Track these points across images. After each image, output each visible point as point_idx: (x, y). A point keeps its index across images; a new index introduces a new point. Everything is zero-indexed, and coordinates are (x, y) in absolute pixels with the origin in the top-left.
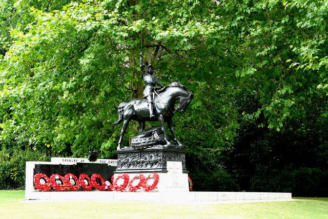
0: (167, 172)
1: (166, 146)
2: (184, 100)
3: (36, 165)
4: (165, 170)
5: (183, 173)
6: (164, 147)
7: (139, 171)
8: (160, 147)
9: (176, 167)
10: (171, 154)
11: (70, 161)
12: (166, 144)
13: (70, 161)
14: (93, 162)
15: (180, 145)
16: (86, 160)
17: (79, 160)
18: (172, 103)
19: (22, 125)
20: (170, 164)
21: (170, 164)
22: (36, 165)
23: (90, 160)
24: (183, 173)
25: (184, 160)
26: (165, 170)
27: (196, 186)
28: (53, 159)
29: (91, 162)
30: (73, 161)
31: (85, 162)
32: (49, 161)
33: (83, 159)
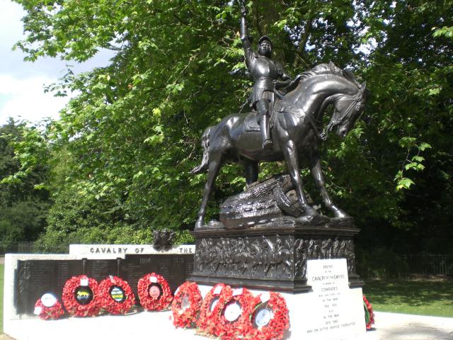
0: (308, 289)
1: (305, 219)
2: (349, 102)
3: (20, 263)
4: (300, 285)
5: (351, 286)
6: (298, 223)
7: (257, 285)
8: (292, 223)
9: (329, 273)
10: (316, 238)
11: (98, 251)
12: (304, 213)
13: (109, 251)
14: (165, 253)
15: (341, 215)
16: (149, 249)
17: (132, 249)
18: (289, 118)
19: (378, 8)
20: (315, 268)
21: (315, 268)
22: (20, 263)
23: (157, 248)
24: (351, 286)
25: (352, 255)
26: (300, 285)
27: (373, 323)
28: (72, 247)
29: (160, 253)
30: (117, 250)
31: (144, 253)
32: (66, 251)
33: (139, 247)
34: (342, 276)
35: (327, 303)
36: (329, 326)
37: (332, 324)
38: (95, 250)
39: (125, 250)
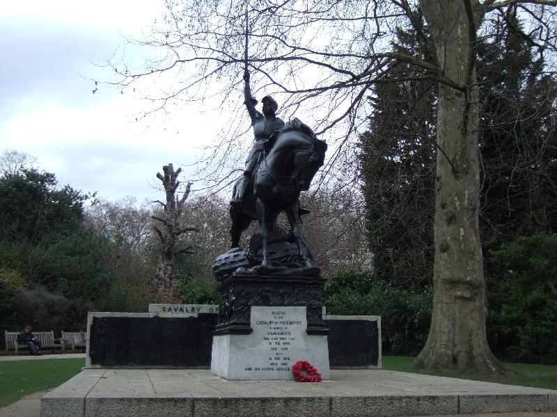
30: (189, 309)
34: (299, 323)
35: (274, 345)
36: (275, 367)
37: (280, 366)
38: (167, 310)
39: (198, 310)
